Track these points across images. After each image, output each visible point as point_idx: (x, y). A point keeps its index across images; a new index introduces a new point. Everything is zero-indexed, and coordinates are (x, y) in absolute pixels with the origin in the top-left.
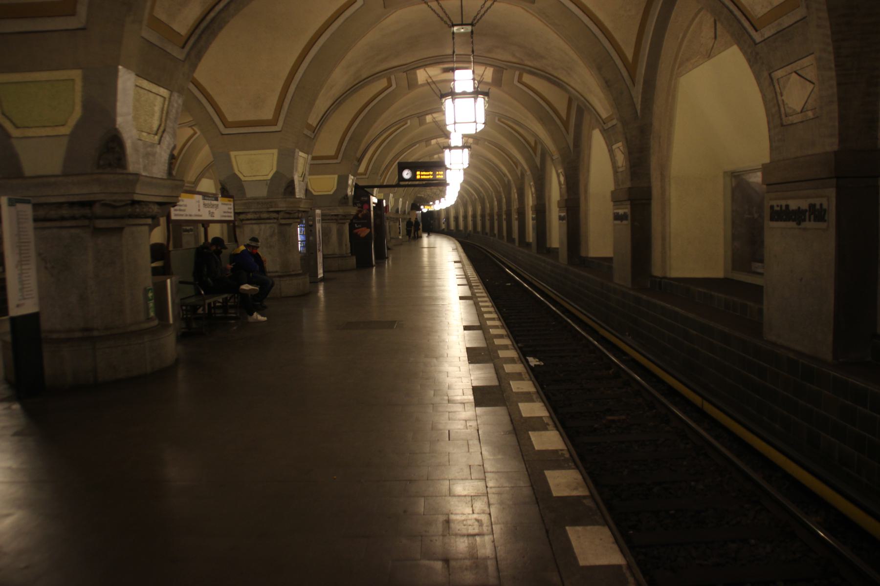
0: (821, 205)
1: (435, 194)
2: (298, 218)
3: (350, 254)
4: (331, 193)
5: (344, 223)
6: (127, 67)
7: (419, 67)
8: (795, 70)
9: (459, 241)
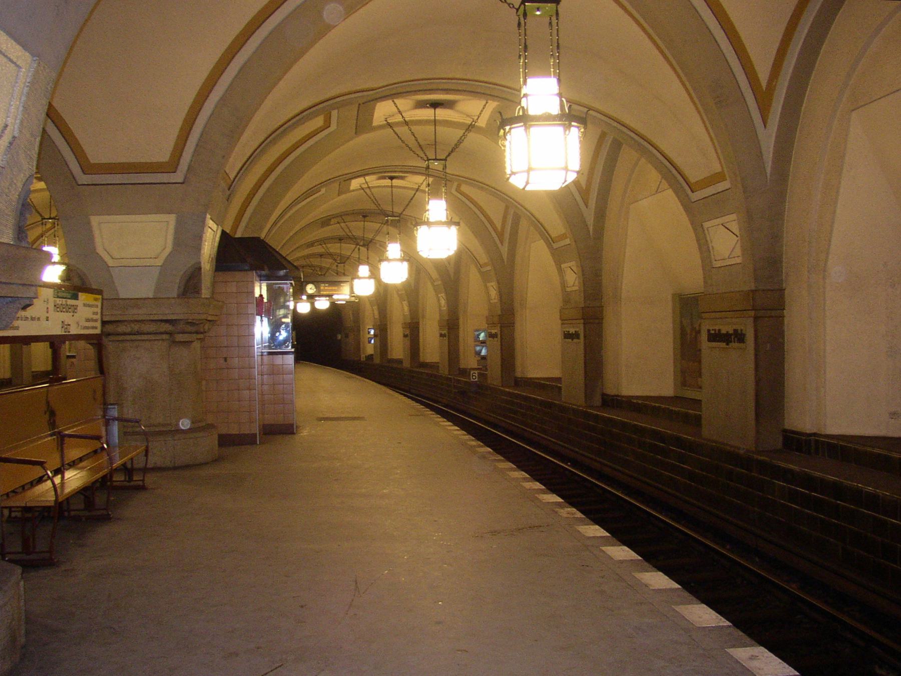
0: (742, 330)
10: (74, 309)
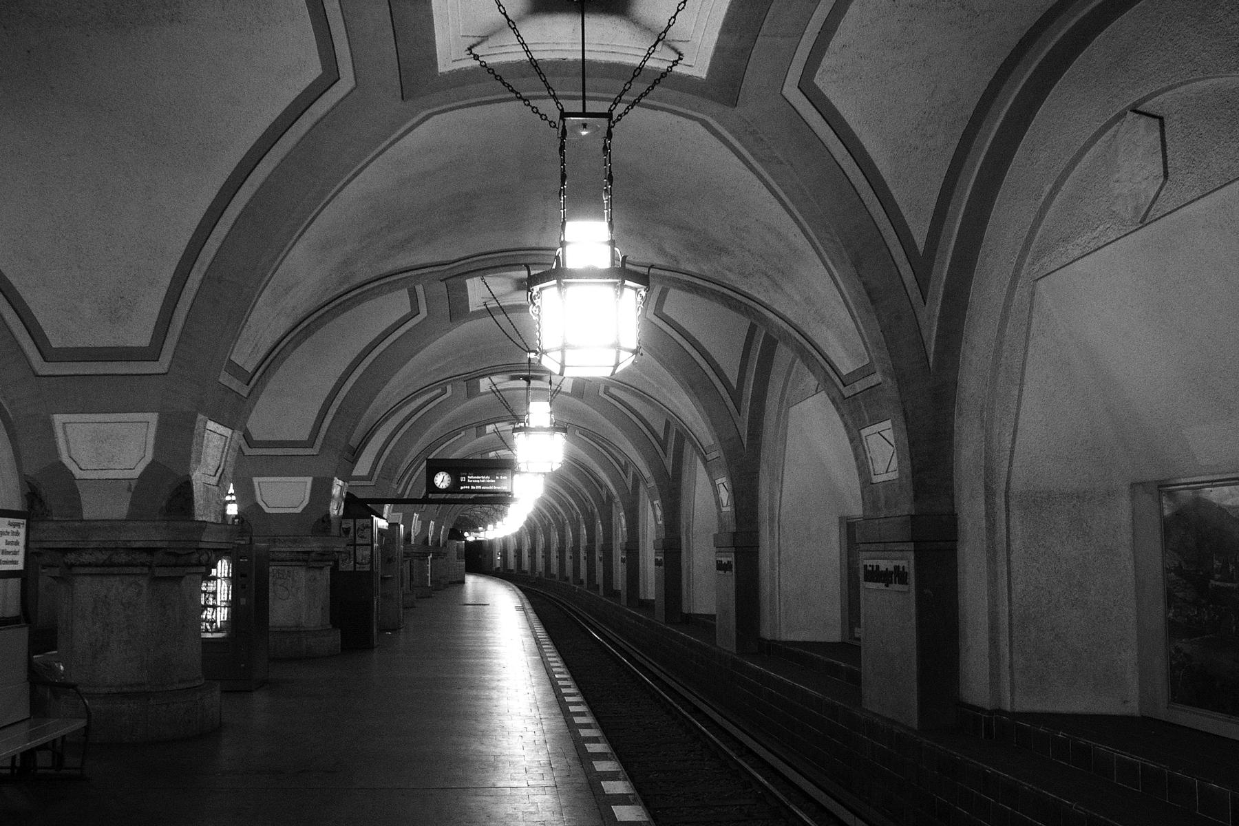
0: (903, 567)
1: (487, 514)
2: (199, 564)
3: (330, 627)
4: (299, 510)
7: (471, 273)
9: (520, 588)
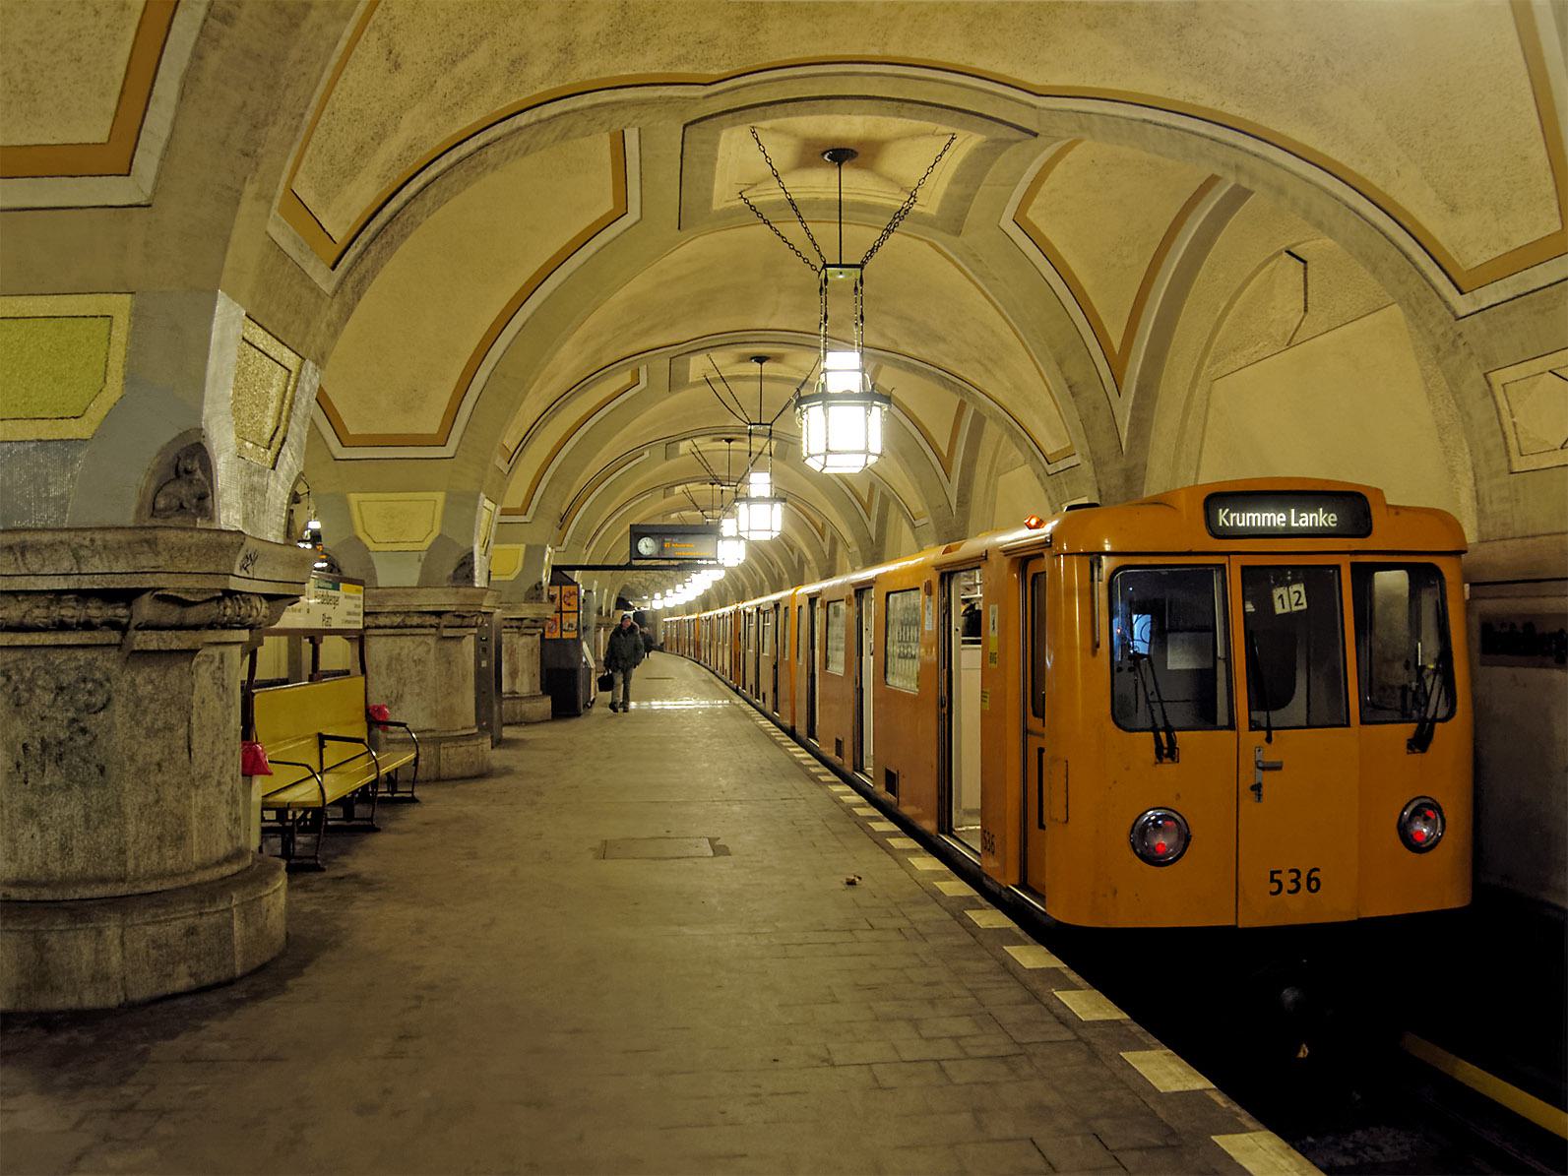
5: (459, 639)
6: (233, 295)
8: (1551, 368)
10: (335, 601)
